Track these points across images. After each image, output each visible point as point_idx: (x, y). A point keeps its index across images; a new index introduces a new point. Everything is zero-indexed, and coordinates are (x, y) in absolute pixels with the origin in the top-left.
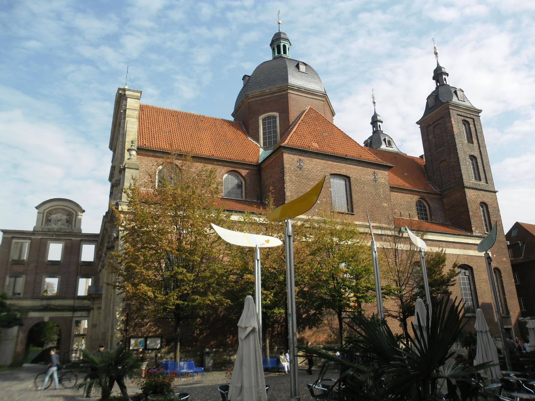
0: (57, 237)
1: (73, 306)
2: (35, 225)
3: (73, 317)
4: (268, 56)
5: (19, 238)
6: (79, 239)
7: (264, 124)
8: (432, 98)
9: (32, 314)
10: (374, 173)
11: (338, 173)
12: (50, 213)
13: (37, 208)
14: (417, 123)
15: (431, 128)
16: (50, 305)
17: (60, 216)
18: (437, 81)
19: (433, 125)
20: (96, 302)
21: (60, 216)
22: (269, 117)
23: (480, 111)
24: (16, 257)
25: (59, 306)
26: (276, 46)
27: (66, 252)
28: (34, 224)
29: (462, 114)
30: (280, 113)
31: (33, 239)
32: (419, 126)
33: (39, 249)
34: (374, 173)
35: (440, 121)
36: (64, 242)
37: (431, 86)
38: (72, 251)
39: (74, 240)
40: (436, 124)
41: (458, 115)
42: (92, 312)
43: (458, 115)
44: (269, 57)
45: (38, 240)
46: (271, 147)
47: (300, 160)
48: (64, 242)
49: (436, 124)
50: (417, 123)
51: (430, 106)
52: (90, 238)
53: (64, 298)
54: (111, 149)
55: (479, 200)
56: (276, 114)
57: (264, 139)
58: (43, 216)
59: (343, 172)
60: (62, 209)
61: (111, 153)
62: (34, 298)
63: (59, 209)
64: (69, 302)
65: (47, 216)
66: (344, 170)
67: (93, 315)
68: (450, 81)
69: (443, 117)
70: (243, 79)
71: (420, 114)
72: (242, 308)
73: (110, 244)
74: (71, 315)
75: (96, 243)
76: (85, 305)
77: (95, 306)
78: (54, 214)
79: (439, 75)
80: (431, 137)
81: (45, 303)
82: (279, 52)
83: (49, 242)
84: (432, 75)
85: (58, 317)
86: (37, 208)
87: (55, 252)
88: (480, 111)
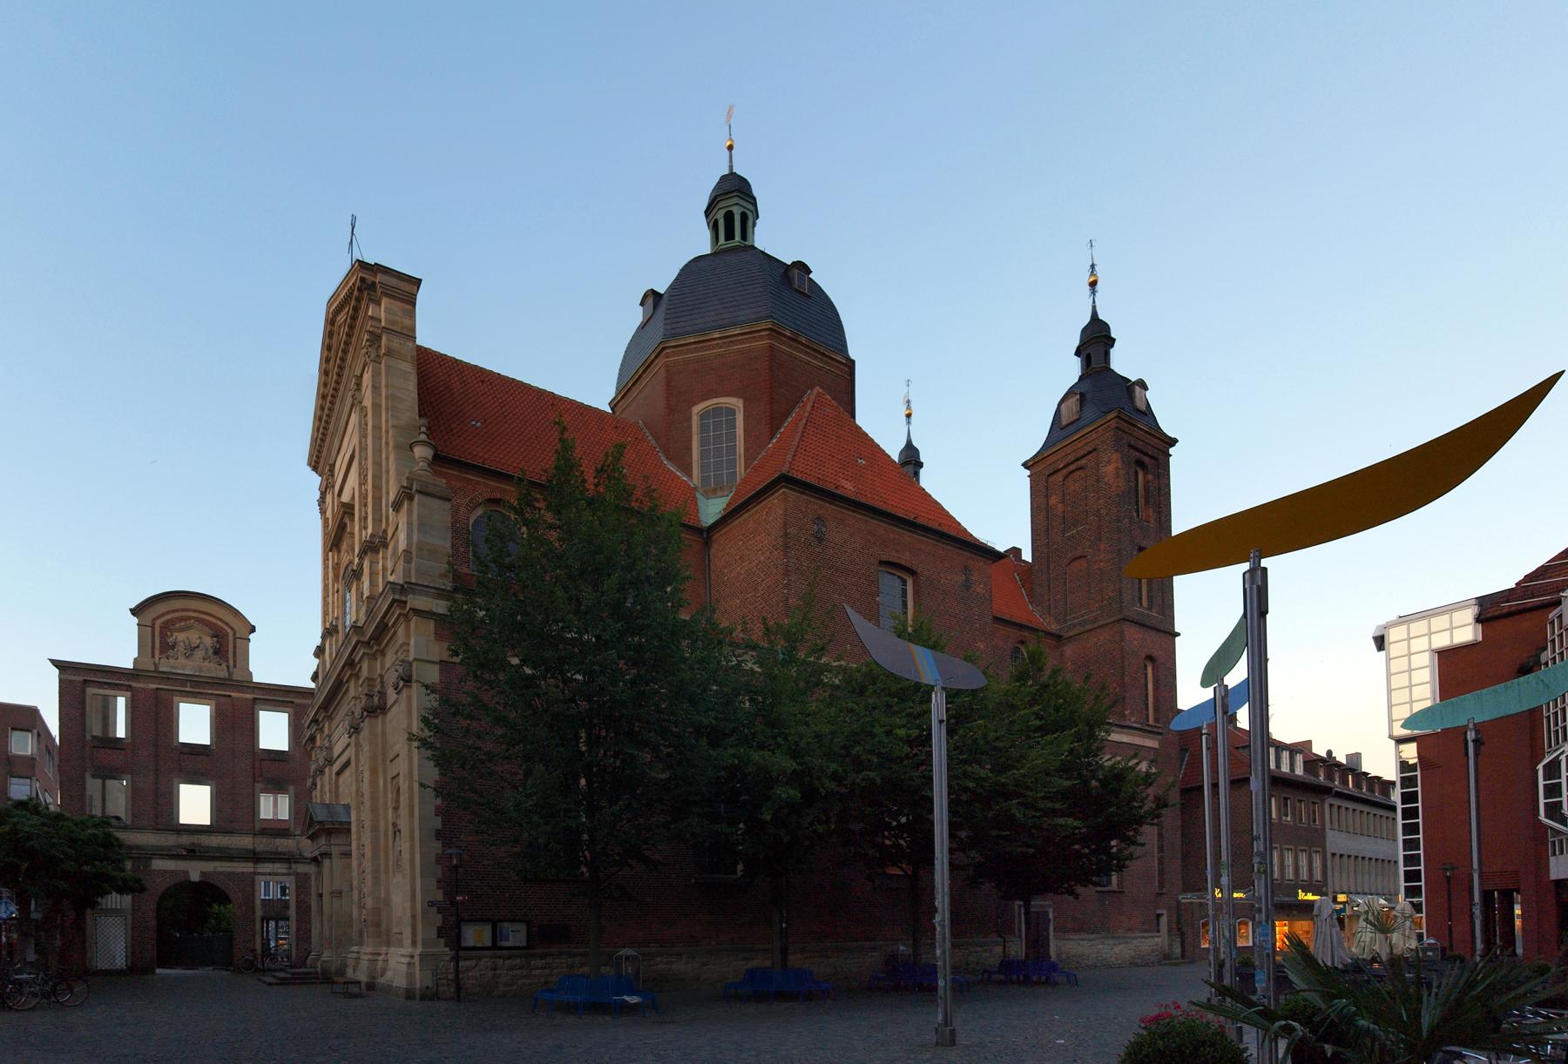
0: (196, 690)
4: (700, 243)
5: (101, 685)
8: (1073, 401)
9: (158, 864)
12: (167, 627)
13: (134, 612)
14: (1026, 465)
15: (1059, 477)
16: (200, 846)
17: (192, 634)
19: (1065, 471)
21: (192, 634)
22: (717, 411)
23: (1173, 442)
25: (219, 849)
26: (720, 216)
27: (220, 723)
29: (1140, 444)
30: (746, 400)
33: (155, 717)
35: (1083, 462)
37: (1070, 371)
39: (239, 703)
40: (1073, 467)
41: (1131, 446)
42: (326, 862)
43: (1131, 446)
45: (153, 691)
49: (1073, 467)
51: (1064, 422)
52: (279, 696)
54: (315, 469)
55: (1146, 651)
57: (704, 468)
59: (905, 558)
60: (197, 619)
61: (315, 480)
62: (157, 829)
63: (190, 618)
65: (163, 636)
68: (1123, 362)
73: (376, 699)
77: (335, 851)
80: (1053, 501)
82: (730, 235)
84: (1076, 342)
85: (222, 873)
86: (134, 612)
87: (194, 724)
88: (1173, 442)
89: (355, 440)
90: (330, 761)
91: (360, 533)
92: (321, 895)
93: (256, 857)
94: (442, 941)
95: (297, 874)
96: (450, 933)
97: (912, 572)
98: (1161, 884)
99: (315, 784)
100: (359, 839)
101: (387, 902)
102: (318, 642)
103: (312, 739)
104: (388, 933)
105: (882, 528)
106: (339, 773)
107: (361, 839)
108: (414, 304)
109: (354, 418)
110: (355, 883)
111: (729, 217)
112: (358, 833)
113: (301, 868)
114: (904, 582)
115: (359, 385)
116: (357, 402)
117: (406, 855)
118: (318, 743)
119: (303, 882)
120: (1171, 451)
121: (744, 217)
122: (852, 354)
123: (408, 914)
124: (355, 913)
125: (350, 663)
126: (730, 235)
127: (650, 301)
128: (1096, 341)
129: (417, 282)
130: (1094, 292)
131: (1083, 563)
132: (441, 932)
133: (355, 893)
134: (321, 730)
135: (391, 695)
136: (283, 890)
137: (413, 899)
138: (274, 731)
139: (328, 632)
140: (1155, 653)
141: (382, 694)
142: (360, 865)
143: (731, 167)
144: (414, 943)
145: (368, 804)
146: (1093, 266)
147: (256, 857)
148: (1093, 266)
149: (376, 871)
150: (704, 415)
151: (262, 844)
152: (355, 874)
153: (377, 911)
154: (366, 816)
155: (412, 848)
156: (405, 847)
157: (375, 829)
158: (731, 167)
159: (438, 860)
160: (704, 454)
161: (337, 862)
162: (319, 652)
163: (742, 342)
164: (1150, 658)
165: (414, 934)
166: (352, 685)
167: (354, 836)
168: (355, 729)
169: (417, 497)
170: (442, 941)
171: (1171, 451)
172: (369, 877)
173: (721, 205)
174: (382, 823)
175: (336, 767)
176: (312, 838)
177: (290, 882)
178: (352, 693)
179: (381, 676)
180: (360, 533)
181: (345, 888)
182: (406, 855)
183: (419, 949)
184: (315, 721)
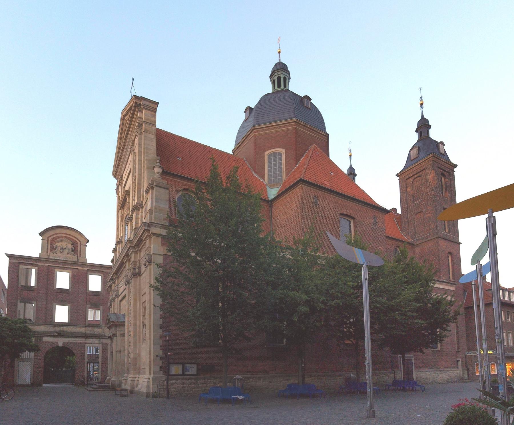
0: (64, 266)
1: (85, 334)
2: (40, 252)
3: (85, 343)
6: (86, 269)
7: (269, 160)
9: (46, 339)
10: (375, 216)
11: (346, 213)
12: (53, 241)
14: (397, 175)
15: (411, 180)
16: (63, 331)
18: (420, 135)
19: (413, 178)
20: (118, 329)
22: (275, 154)
23: (456, 166)
24: (23, 284)
25: (71, 333)
26: (276, 78)
27: (73, 280)
28: (39, 251)
31: (40, 266)
32: (398, 178)
33: (47, 278)
34: (375, 216)
35: (420, 174)
36: (71, 271)
37: (414, 138)
38: (79, 281)
39: (81, 271)
41: (439, 168)
42: (115, 338)
43: (439, 168)
44: (268, 89)
45: (46, 266)
46: (277, 185)
47: (315, 196)
48: (71, 271)
50: (397, 175)
51: (412, 158)
52: (97, 269)
53: (75, 326)
54: (115, 177)
55: (448, 250)
56: (282, 151)
57: (269, 176)
58: (48, 244)
59: (350, 213)
61: (115, 181)
62: (46, 324)
63: (63, 237)
64: (81, 330)
65: (52, 244)
66: (351, 211)
67: (117, 341)
68: (434, 134)
69: (425, 169)
70: (245, 112)
71: (400, 164)
72: (68, 348)
73: (137, 270)
74: (84, 342)
75: (102, 274)
76: (96, 333)
77: (118, 334)
78: (59, 242)
79: (423, 126)
80: (409, 189)
81: (57, 329)
82: (279, 86)
83: (56, 270)
84: (415, 127)
87: (63, 280)
88: (456, 166)
89: (131, 165)
90: (117, 296)
91: (132, 202)
92: (112, 353)
93: (86, 336)
94: (162, 372)
95: (103, 343)
96: (165, 369)
97: (353, 218)
98: (458, 348)
99: (111, 305)
100: (128, 328)
101: (139, 355)
102: (114, 246)
103: (111, 286)
104: (139, 368)
105: (340, 200)
106: (121, 301)
107: (129, 329)
108: (156, 112)
109: (131, 157)
110: (126, 347)
111: (279, 79)
112: (128, 326)
113: (104, 341)
114: (350, 222)
115: (133, 144)
116: (132, 150)
117: (147, 335)
118: (113, 288)
119: (105, 347)
120: (455, 169)
121: (285, 79)
122: (328, 131)
123: (148, 360)
124: (126, 360)
125: (127, 255)
126: (279, 86)
127: (248, 111)
128: (423, 126)
129: (157, 104)
130: (422, 107)
131: (422, 214)
132: (161, 368)
133: (126, 351)
134: (114, 283)
135: (143, 268)
136: (97, 350)
137: (150, 354)
138: (95, 283)
139: (118, 243)
140: (452, 251)
141: (140, 268)
142: (128, 340)
143: (280, 60)
144: (150, 373)
145: (132, 314)
146: (421, 97)
147: (86, 336)
148: (421, 97)
149: (135, 342)
150: (269, 156)
151: (89, 331)
152: (126, 343)
153: (135, 359)
154: (132, 319)
155: (150, 332)
156: (147, 332)
157: (135, 324)
158: (280, 60)
159: (161, 337)
160: (269, 171)
161: (119, 338)
162: (114, 251)
163: (284, 127)
164: (450, 253)
165: (150, 369)
166: (127, 264)
167: (126, 327)
168: (128, 282)
169: (155, 188)
170: (162, 372)
171: (455, 169)
172: (132, 345)
173: (276, 74)
174: (138, 322)
175: (120, 298)
176: (109, 328)
177: (100, 347)
178: (127, 267)
179: (139, 261)
180: (132, 202)
181: (122, 349)
182: (147, 335)
183: (152, 376)
184: (112, 279)
